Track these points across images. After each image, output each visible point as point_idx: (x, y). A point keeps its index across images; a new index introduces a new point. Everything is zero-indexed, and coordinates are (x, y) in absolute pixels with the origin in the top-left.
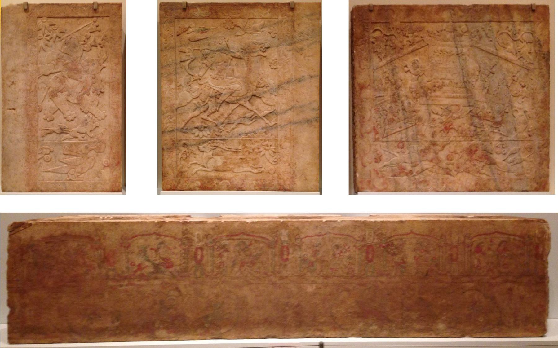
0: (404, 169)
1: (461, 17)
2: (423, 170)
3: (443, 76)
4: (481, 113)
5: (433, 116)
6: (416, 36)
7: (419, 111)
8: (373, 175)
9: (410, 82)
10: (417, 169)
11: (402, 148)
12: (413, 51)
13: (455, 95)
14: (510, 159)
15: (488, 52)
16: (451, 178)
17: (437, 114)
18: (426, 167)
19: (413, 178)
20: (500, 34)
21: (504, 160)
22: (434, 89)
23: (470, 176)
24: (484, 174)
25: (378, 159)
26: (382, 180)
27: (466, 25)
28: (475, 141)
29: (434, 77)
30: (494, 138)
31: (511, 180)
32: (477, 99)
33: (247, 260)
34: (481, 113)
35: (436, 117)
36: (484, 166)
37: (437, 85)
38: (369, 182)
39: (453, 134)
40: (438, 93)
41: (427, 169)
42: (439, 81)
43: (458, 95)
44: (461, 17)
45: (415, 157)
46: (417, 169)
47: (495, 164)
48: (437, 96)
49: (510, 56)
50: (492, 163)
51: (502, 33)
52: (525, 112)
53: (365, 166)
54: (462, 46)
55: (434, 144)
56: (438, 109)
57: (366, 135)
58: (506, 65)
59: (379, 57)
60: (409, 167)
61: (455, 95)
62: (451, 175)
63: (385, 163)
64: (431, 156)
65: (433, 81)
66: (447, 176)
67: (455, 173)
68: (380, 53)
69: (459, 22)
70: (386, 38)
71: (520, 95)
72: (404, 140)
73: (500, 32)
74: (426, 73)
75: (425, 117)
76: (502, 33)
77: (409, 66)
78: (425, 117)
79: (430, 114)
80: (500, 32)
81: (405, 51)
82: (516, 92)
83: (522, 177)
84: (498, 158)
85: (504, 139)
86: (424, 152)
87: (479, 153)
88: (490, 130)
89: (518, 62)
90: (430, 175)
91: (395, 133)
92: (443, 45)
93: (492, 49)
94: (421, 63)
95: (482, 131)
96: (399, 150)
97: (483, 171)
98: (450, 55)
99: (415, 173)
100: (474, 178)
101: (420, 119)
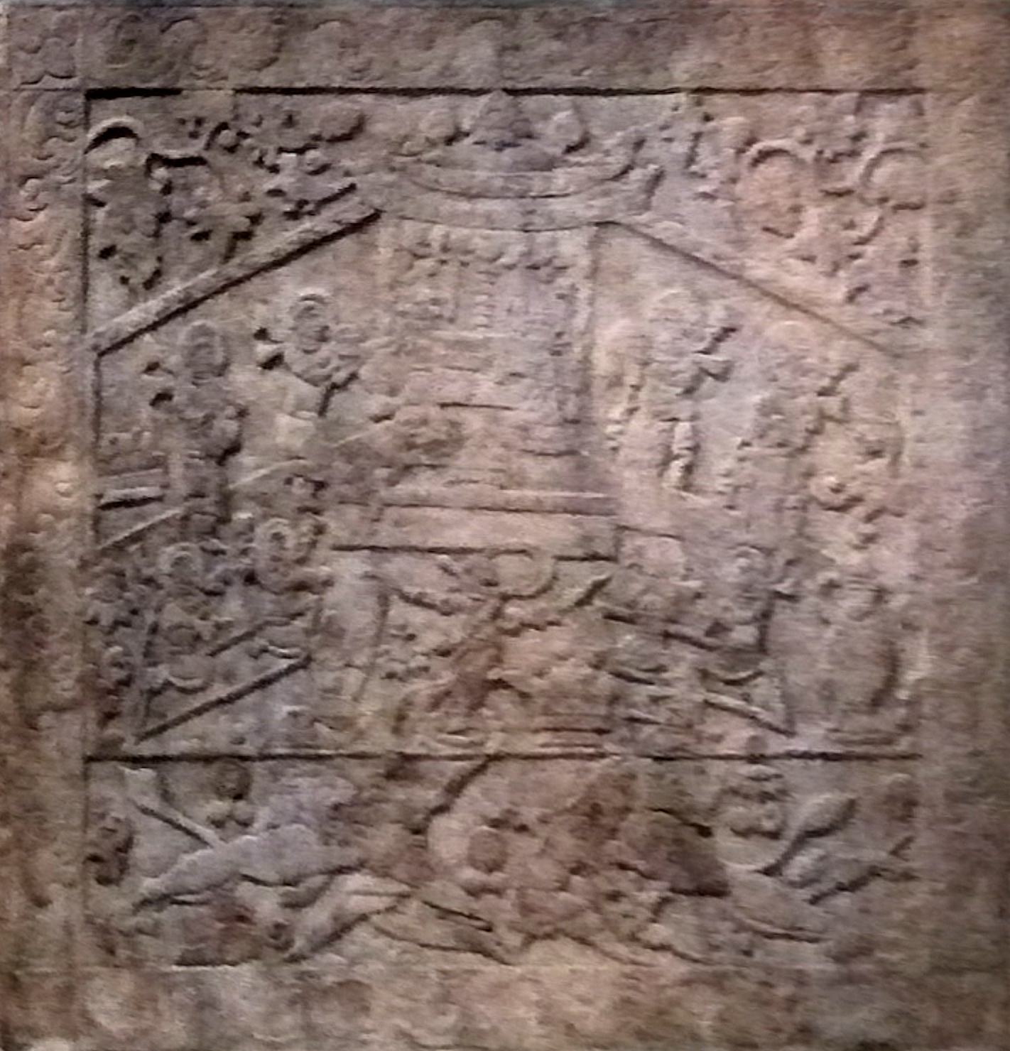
0: (242, 918)
1: (550, 61)
2: (341, 929)
3: (454, 391)
4: (648, 598)
5: (399, 611)
6: (322, 169)
7: (328, 583)
8: (86, 949)
9: (283, 420)
10: (318, 917)
11: (238, 797)
12: (306, 248)
13: (513, 493)
14: (804, 861)
15: (689, 258)
16: (492, 970)
17: (418, 602)
18: (356, 904)
19: (287, 973)
20: (756, 162)
21: (768, 871)
22: (407, 457)
23: (586, 962)
24: (663, 948)
25: (111, 862)
26: (127, 983)
27: (577, 109)
28: (617, 756)
29: (407, 393)
30: (718, 739)
31: (801, 979)
32: (637, 520)
33: (841, 855)
34: (648, 598)
35: (418, 616)
36: (665, 901)
37: (425, 435)
38: (67, 993)
39: (501, 725)
40: (424, 484)
41: (363, 918)
42: (434, 412)
43: (530, 494)
44: (550, 61)
45: (306, 848)
46: (318, 917)
47: (719, 891)
48: (417, 503)
49: (800, 279)
50: (710, 887)
51: (765, 155)
52: (881, 595)
53: (41, 903)
54: (556, 225)
55: (402, 768)
56: (425, 577)
57: (46, 720)
58: (781, 327)
59: (124, 280)
60: (267, 906)
61: (513, 493)
62: (488, 954)
63: (149, 885)
64: (385, 838)
65: (401, 416)
66: (470, 960)
67: (514, 940)
68: (129, 259)
69: (544, 91)
70: (161, 172)
71: (856, 500)
72: (248, 749)
73: (753, 151)
74: (364, 372)
75: (360, 619)
76: (765, 155)
77: (277, 332)
78: (360, 619)
79: (384, 601)
80: (753, 151)
81: (263, 247)
82: (832, 480)
83: (863, 966)
84: (740, 862)
85: (776, 744)
86: (343, 818)
87: (638, 824)
88: (699, 697)
89: (847, 316)
90: (377, 955)
91: (198, 712)
92: (454, 219)
93: (710, 243)
94: (348, 316)
95: (656, 700)
96: (219, 806)
97: (660, 932)
98: (494, 267)
99: (299, 944)
100: (609, 969)
101: (330, 631)
